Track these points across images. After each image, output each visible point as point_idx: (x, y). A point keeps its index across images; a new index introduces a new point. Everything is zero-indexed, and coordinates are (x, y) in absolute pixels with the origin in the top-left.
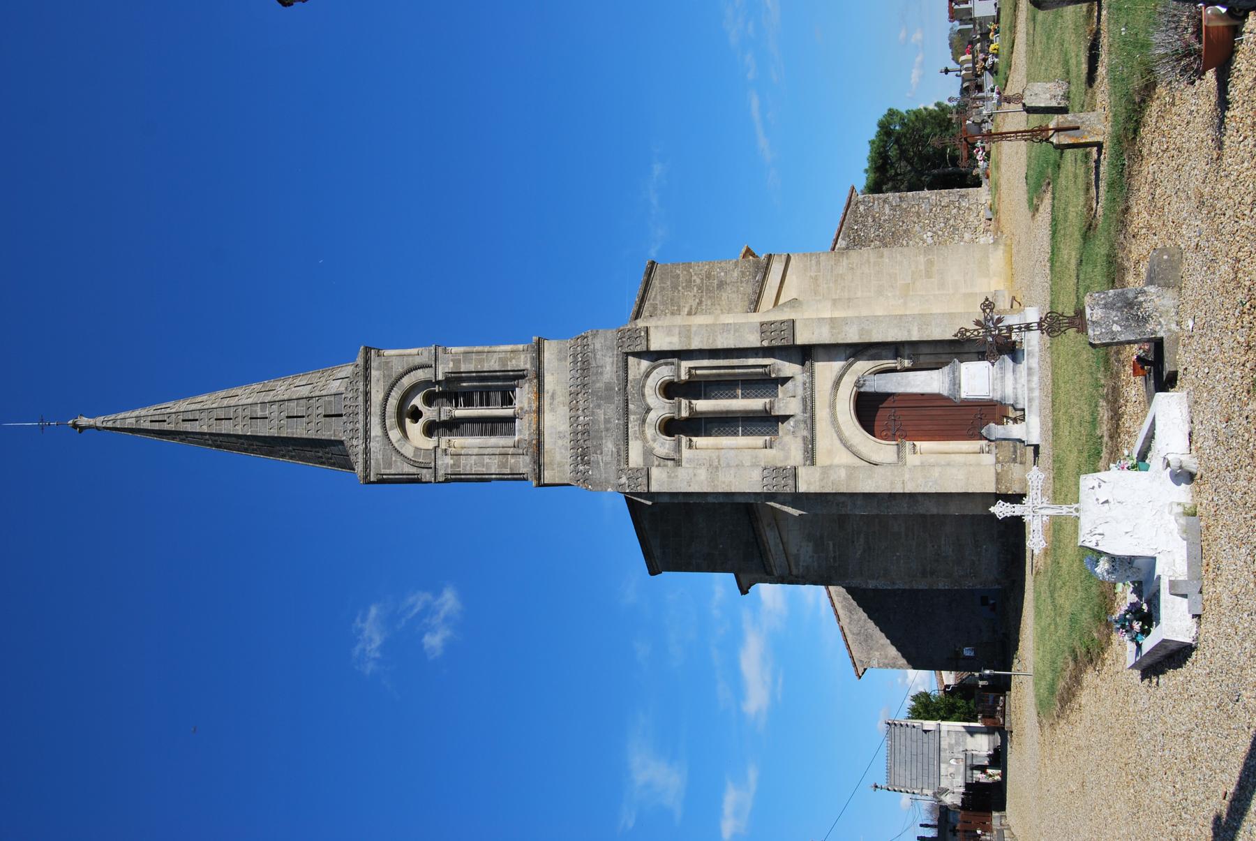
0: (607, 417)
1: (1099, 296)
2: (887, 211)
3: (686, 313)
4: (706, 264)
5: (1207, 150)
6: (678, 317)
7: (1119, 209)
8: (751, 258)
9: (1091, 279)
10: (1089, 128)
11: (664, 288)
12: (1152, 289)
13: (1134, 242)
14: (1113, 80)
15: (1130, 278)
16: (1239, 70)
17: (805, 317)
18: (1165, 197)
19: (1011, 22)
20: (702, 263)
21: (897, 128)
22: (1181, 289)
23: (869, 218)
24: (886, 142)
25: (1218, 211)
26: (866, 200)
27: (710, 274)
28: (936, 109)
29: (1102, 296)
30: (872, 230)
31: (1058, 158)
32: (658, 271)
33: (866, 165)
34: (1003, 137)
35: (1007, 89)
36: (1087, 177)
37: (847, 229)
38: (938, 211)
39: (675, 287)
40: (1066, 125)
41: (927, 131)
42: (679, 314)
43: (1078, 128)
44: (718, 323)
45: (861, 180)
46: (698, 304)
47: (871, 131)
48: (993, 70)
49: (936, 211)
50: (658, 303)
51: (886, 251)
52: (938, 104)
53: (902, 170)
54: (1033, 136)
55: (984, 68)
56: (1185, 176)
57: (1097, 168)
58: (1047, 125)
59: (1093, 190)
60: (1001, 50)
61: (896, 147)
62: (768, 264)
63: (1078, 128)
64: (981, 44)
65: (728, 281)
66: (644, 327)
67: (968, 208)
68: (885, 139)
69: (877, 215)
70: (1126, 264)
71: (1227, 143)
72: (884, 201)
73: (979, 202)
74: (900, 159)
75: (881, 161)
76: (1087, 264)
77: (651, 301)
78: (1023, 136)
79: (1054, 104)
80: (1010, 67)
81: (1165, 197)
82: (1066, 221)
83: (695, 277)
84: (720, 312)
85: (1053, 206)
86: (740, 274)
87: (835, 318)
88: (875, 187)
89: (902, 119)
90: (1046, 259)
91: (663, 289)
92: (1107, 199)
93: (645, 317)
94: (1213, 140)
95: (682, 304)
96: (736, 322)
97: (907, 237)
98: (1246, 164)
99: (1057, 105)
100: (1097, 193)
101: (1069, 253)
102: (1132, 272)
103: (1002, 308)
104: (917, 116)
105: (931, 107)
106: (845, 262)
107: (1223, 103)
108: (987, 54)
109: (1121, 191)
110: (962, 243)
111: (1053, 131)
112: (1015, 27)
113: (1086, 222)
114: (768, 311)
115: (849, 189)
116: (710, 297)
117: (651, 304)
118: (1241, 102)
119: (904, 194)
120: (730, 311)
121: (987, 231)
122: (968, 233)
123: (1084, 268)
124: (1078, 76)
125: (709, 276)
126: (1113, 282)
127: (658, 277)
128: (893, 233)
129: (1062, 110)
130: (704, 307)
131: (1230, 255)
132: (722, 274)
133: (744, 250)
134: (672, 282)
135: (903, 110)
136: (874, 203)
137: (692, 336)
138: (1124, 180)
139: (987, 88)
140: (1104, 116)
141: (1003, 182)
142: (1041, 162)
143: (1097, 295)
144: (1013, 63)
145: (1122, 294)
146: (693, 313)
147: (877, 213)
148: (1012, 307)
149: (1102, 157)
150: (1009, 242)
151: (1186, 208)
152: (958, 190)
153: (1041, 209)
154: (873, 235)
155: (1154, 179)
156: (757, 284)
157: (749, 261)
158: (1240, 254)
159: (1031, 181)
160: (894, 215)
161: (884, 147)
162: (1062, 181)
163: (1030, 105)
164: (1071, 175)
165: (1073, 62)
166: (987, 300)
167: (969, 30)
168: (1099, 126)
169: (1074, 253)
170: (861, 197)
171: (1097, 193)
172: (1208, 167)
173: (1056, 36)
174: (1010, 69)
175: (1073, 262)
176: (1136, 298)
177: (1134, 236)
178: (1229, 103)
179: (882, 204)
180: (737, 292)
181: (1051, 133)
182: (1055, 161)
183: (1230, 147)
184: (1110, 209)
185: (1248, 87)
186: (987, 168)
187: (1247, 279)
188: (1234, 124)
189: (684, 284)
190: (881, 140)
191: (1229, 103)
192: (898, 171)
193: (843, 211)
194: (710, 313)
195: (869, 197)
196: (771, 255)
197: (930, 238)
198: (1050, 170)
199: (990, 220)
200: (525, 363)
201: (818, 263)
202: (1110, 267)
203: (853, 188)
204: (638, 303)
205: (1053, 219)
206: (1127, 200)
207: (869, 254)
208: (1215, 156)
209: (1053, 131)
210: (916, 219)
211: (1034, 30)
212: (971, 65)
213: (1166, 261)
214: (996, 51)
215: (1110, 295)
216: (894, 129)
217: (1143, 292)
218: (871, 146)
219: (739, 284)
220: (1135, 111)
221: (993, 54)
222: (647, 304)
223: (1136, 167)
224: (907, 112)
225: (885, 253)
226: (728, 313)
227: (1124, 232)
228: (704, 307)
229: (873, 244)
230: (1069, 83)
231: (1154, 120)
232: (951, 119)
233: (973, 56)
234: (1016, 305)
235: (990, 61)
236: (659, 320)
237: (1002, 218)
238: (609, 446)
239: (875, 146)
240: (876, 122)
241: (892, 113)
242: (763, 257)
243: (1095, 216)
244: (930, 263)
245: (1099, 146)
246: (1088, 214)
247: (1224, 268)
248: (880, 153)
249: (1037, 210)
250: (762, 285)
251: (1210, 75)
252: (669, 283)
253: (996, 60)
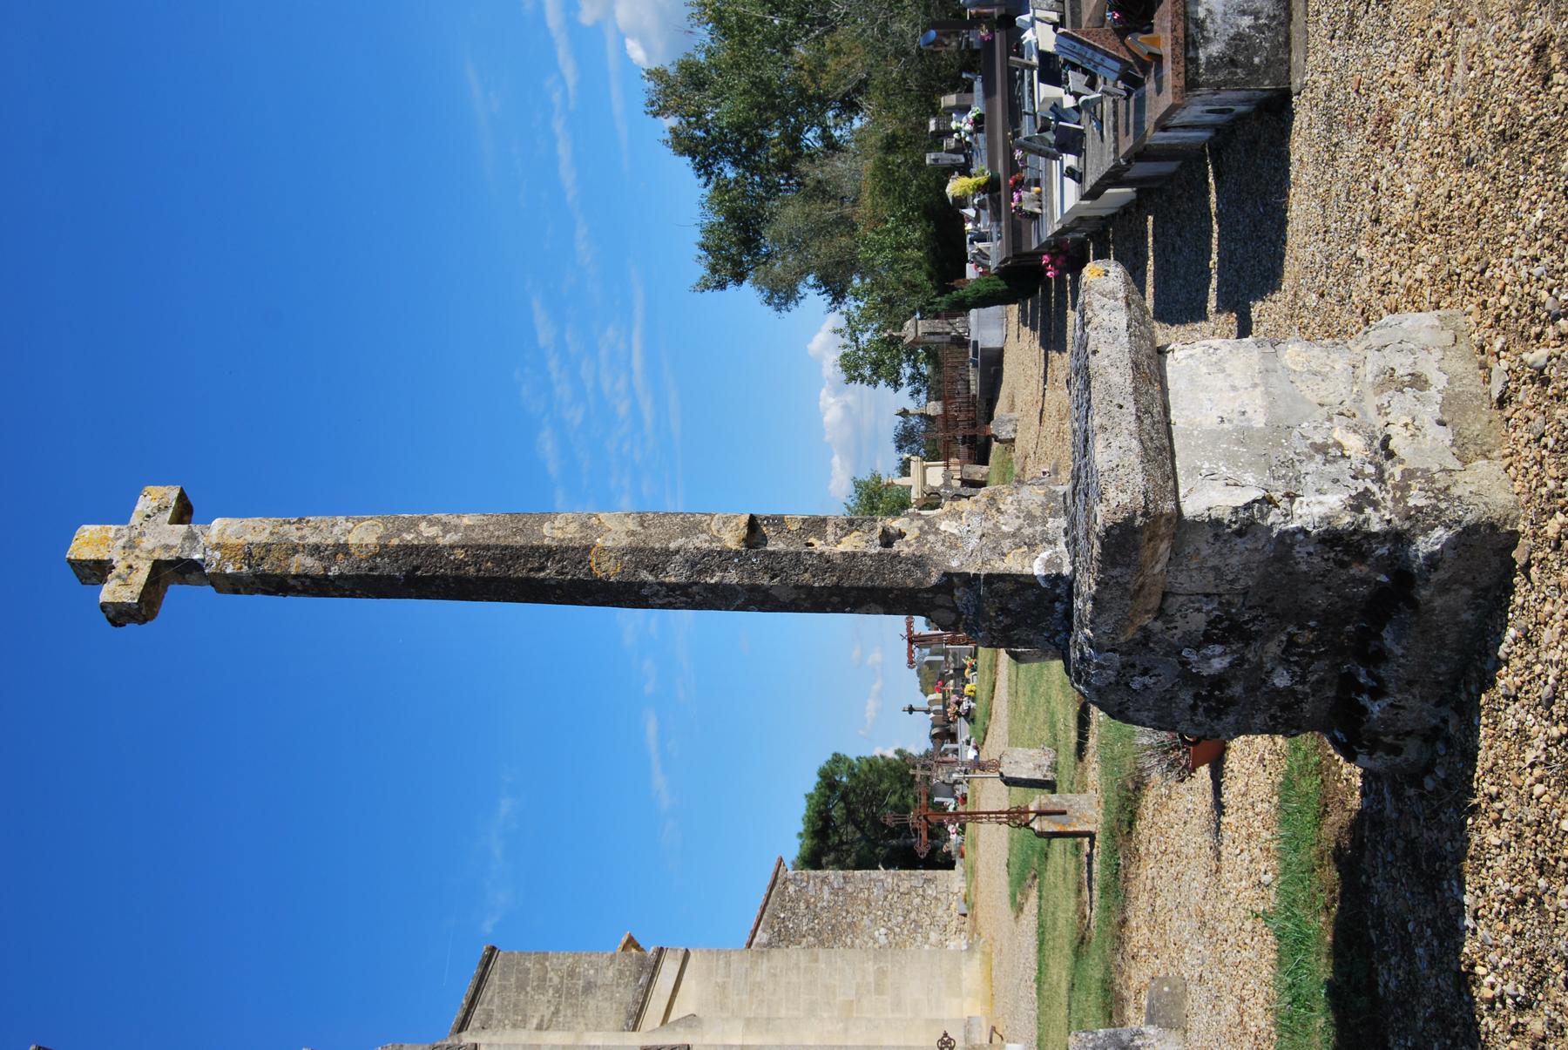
1: (1087, 1037)
2: (826, 895)
3: (534, 1026)
4: (569, 957)
5: (1205, 859)
6: (523, 1031)
7: (1115, 921)
8: (634, 951)
9: (1084, 1010)
10: (1078, 814)
11: (505, 987)
12: (1151, 1030)
13: (1134, 965)
14: (1103, 760)
15: (1130, 1012)
16: (1232, 771)
17: (705, 1042)
18: (1165, 911)
19: (991, 660)
20: (564, 954)
21: (844, 779)
22: (1186, 1032)
23: (801, 904)
24: (829, 797)
25: (1220, 937)
26: (798, 877)
27: (573, 971)
28: (897, 757)
29: (1090, 1037)
30: (805, 921)
31: (1045, 845)
32: (499, 961)
33: (801, 827)
34: (973, 818)
35: (986, 743)
36: (1078, 875)
37: (769, 917)
38: (895, 899)
39: (521, 987)
40: (1050, 808)
41: (885, 785)
42: (524, 1028)
43: (1064, 813)
44: (580, 1044)
45: (792, 847)
46: (553, 1013)
47: (810, 782)
48: (969, 716)
49: (892, 899)
50: (494, 1008)
51: (822, 953)
52: (899, 752)
53: (849, 838)
54: (1009, 818)
55: (958, 714)
56: (1184, 889)
57: (1090, 864)
58: (1027, 807)
59: (1086, 892)
60: (978, 693)
61: (842, 805)
62: (657, 962)
63: (1064, 813)
64: (955, 682)
65: (599, 983)
66: (472, 1044)
67: (936, 898)
68: (828, 793)
69: (812, 900)
70: (1125, 993)
71: (1224, 853)
72: (823, 881)
73: (951, 890)
74: (846, 822)
75: (820, 823)
76: (1079, 990)
77: (485, 1006)
78: (997, 818)
79: (1038, 776)
80: (990, 715)
81: (1165, 911)
82: (1055, 930)
83: (552, 973)
84: (584, 1028)
85: (1040, 908)
86: (617, 973)
87: (748, 1046)
88: (812, 860)
89: (851, 767)
90: (1033, 978)
91: (503, 988)
92: (1100, 907)
93: (474, 1029)
94: (1211, 848)
95: (529, 1013)
96: (607, 1043)
97: (853, 933)
98: (1244, 883)
99: (1042, 778)
100: (1091, 897)
101: (1059, 972)
102: (1132, 1004)
103: (978, 1042)
104: (871, 765)
105: (890, 754)
106: (764, 965)
107: (1219, 807)
108: (962, 696)
109: (1117, 897)
110: (927, 947)
111: (1033, 815)
112: (996, 666)
113: (1078, 933)
114: (653, 1031)
115: (776, 861)
116: (571, 1005)
117: (485, 1010)
118: (1235, 808)
119: (849, 873)
120: (598, 1027)
121: (961, 931)
122: (935, 931)
123: (1076, 994)
124: (1066, 745)
125: (572, 974)
126: (1111, 1016)
127: (498, 971)
128: (833, 926)
129: (1050, 786)
130: (561, 1019)
131: (1235, 993)
132: (592, 972)
133: (624, 939)
134: (518, 979)
135: (852, 755)
136: (808, 882)
138: (1120, 884)
139: (962, 738)
140: (1096, 800)
141: (980, 865)
142: (1025, 849)
143: (1083, 1035)
144: (994, 711)
145: (1115, 1034)
146: (545, 1027)
147: (812, 896)
148: (991, 1042)
149: (1095, 851)
150: (988, 949)
151: (1188, 928)
152: (923, 871)
153: (1026, 909)
154: (805, 928)
155: (1154, 887)
156: (640, 990)
157: (631, 955)
158: (1245, 992)
159: (1014, 870)
160: (836, 902)
161: (826, 804)
162: (1050, 876)
163: (1008, 776)
164: (1060, 869)
165: (1060, 726)
166: (946, 1035)
167: (941, 662)
168: (1090, 812)
169: (1064, 974)
170: (791, 873)
171: (1091, 897)
172: (1208, 880)
173: (1041, 690)
174: (990, 719)
175: (1064, 985)
176: (1132, 1041)
177: (1133, 957)
178: (1224, 807)
179: (819, 884)
180: (611, 999)
181: (1031, 816)
182: (1042, 848)
183: (1227, 859)
184: (1106, 921)
185: (1242, 792)
186: (961, 844)
187: (1252, 1024)
188: (1230, 833)
189: (535, 984)
190: (821, 795)
191: (1224, 807)
192: (844, 838)
193: (765, 891)
194: (569, 1029)
195: (802, 874)
196: (662, 948)
197: (883, 937)
198: (1035, 859)
199: (965, 915)
201: (728, 964)
202: (1106, 996)
203: (781, 860)
204: (466, 1006)
205: (1041, 926)
206: (1123, 910)
207: (798, 956)
208: (1214, 868)
209: (1033, 815)
210: (864, 909)
211: (1017, 676)
212: (941, 707)
213: (1167, 994)
214: (972, 694)
215: (1100, 1035)
216: (840, 781)
217: (1140, 1034)
218: (808, 801)
219: (614, 988)
220: (1129, 799)
221: (969, 696)
222: (478, 1010)
223: (1132, 869)
224: (858, 759)
225: (820, 956)
226: (596, 1030)
227: (1121, 951)
228: (561, 1019)
229: (805, 940)
230: (1057, 750)
231: (1150, 814)
232: (914, 776)
233: (944, 696)
234: (996, 1039)
235: (965, 706)
236: (495, 1034)
237: (981, 915)
239: (814, 801)
240: (816, 769)
241: (837, 759)
242: (651, 951)
243: (1088, 927)
244: (881, 973)
245: (1091, 836)
246: (1080, 922)
247: (1231, 1008)
248: (820, 813)
249: (1021, 910)
250: (647, 991)
251: (1204, 771)
252: (513, 980)
253: (973, 705)
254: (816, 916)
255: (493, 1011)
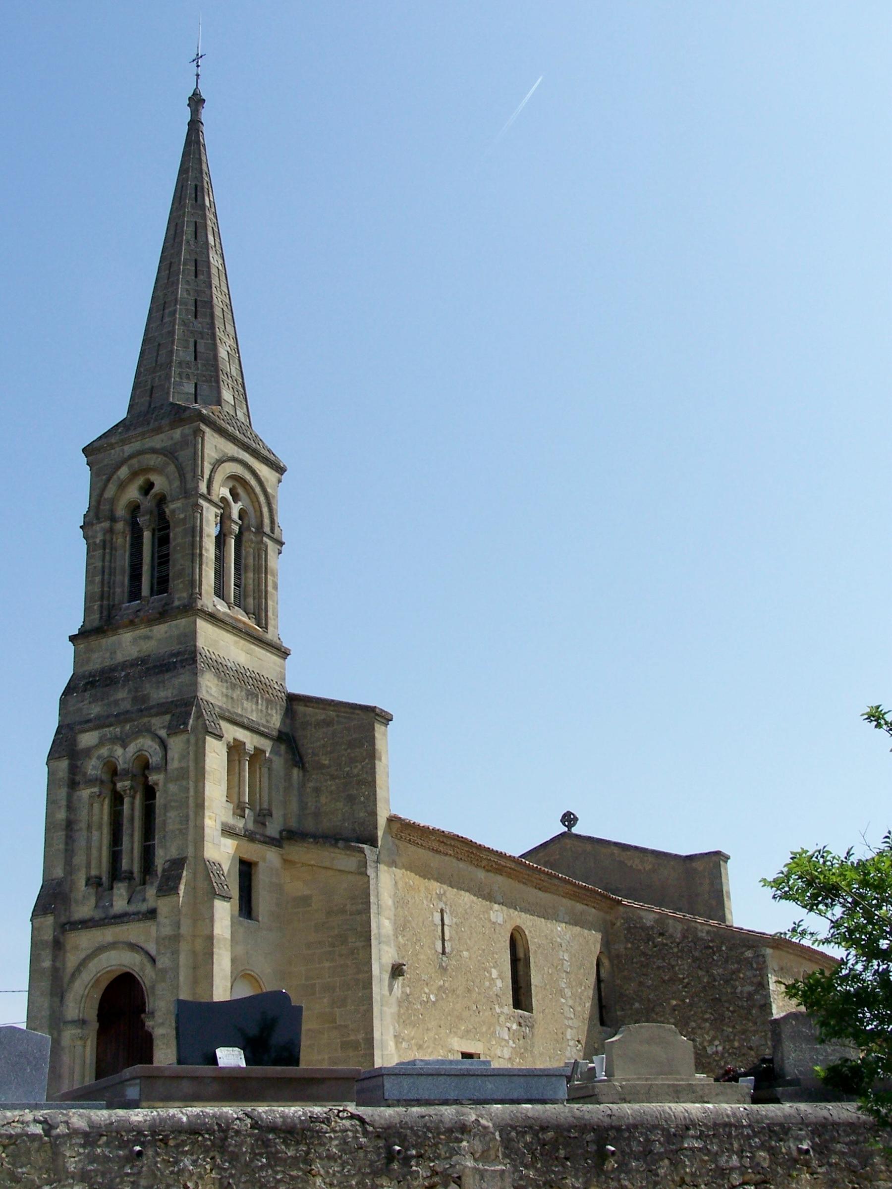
0: (120, 702)
30: (720, 971)
50: (335, 727)
65: (354, 807)
69: (742, 975)
137: (178, 783)
179: (755, 980)
200: (179, 599)
238: (95, 710)
254: (727, 982)
255: (333, 726)
